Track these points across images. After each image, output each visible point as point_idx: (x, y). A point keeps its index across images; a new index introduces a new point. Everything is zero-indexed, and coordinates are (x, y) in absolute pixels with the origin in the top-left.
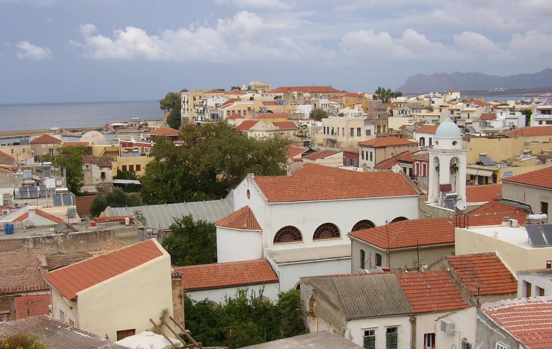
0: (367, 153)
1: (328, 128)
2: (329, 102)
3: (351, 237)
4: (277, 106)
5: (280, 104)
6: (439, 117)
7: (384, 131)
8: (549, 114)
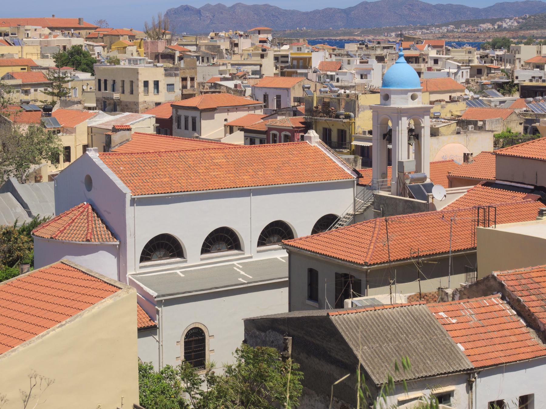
0: (186, 118)
1: (106, 81)
2: (85, 42)
3: (288, 247)
4: (11, 47)
5: (14, 44)
6: (261, 66)
7: (192, 86)
8: (416, 63)
